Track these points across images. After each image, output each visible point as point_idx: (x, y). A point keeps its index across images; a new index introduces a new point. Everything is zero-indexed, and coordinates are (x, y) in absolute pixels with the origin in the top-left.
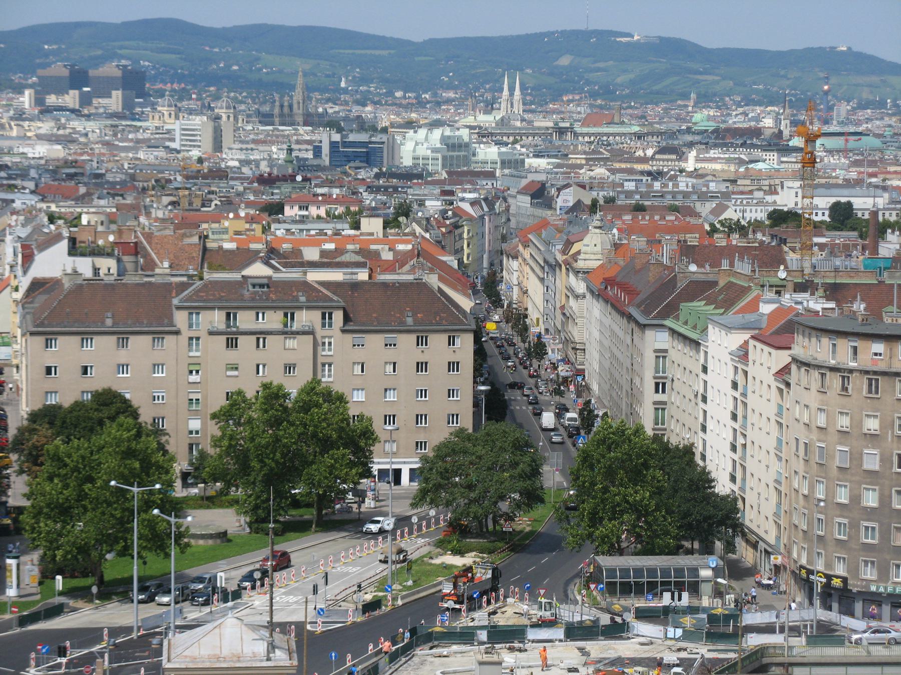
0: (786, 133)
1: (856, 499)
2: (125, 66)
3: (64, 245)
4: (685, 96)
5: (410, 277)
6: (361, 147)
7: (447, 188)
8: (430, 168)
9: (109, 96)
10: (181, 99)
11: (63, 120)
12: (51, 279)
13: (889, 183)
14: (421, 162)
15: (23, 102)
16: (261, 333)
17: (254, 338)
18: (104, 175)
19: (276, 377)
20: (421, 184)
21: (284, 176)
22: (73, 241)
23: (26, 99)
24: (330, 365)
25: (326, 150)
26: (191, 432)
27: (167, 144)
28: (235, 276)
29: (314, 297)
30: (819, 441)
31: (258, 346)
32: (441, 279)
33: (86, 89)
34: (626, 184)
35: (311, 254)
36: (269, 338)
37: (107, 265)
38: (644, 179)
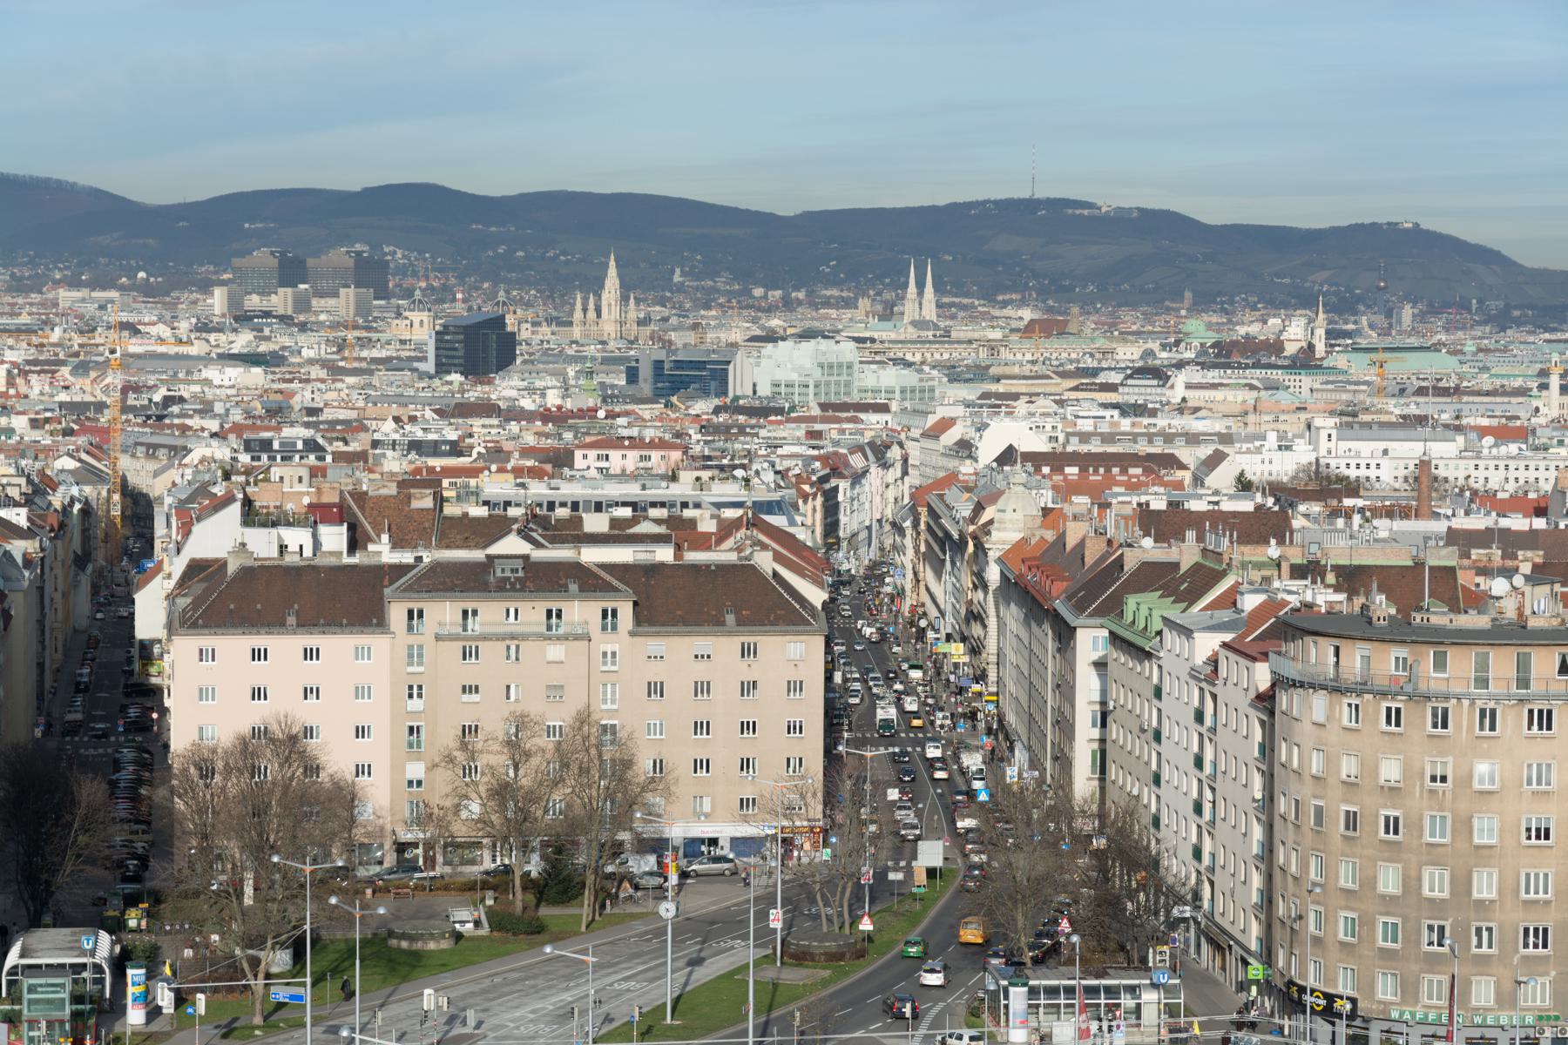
0: (1320, 348)
1: (1411, 883)
2: (359, 254)
3: (235, 509)
4: (1178, 296)
5: (732, 557)
6: (692, 369)
7: (818, 427)
8: (796, 398)
9: (336, 295)
10: (441, 301)
11: (267, 331)
12: (216, 560)
13: (1465, 421)
14: (783, 390)
15: (212, 306)
16: (513, 637)
17: (502, 645)
18: (321, 410)
19: (534, 706)
20: (779, 423)
21: (580, 410)
22: (248, 503)
23: (217, 301)
24: (614, 685)
25: (645, 372)
26: (410, 783)
27: (416, 364)
28: (478, 555)
29: (590, 581)
30: (1315, 797)
31: (508, 658)
32: (778, 558)
33: (302, 286)
34: (1079, 421)
35: (595, 523)
36: (523, 645)
37: (297, 538)
38: (1108, 413)
